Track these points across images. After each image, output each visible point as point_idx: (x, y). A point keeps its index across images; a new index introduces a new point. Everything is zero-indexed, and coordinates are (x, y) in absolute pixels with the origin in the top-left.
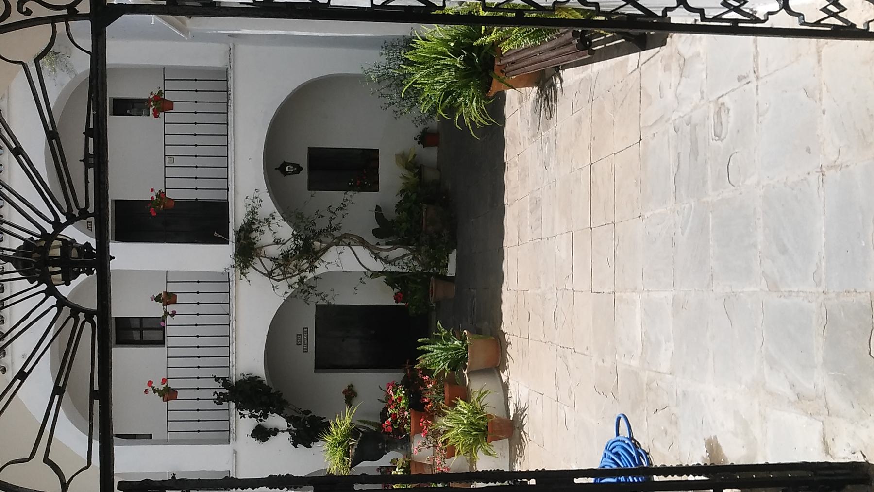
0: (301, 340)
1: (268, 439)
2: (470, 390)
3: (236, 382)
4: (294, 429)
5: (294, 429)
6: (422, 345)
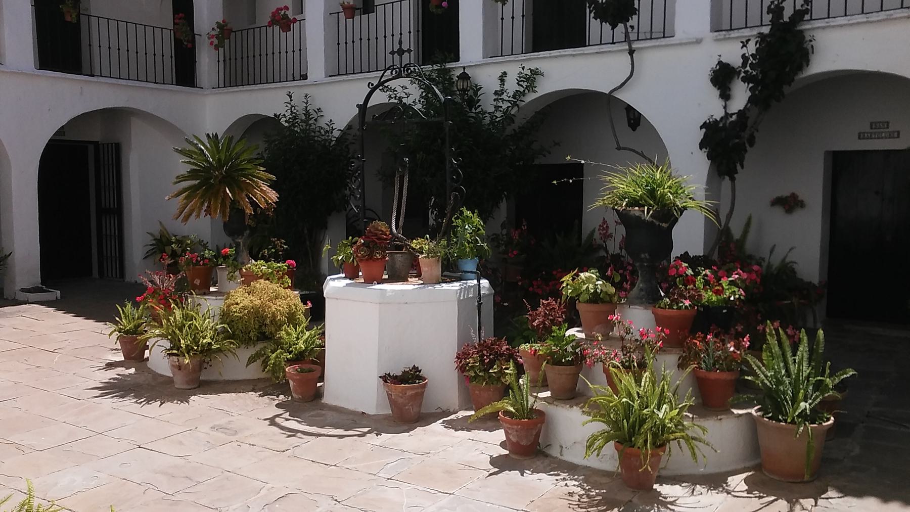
0: (878, 128)
1: (715, 87)
2: (719, 417)
3: (802, 32)
4: (728, 122)
5: (728, 122)
6: (809, 339)
